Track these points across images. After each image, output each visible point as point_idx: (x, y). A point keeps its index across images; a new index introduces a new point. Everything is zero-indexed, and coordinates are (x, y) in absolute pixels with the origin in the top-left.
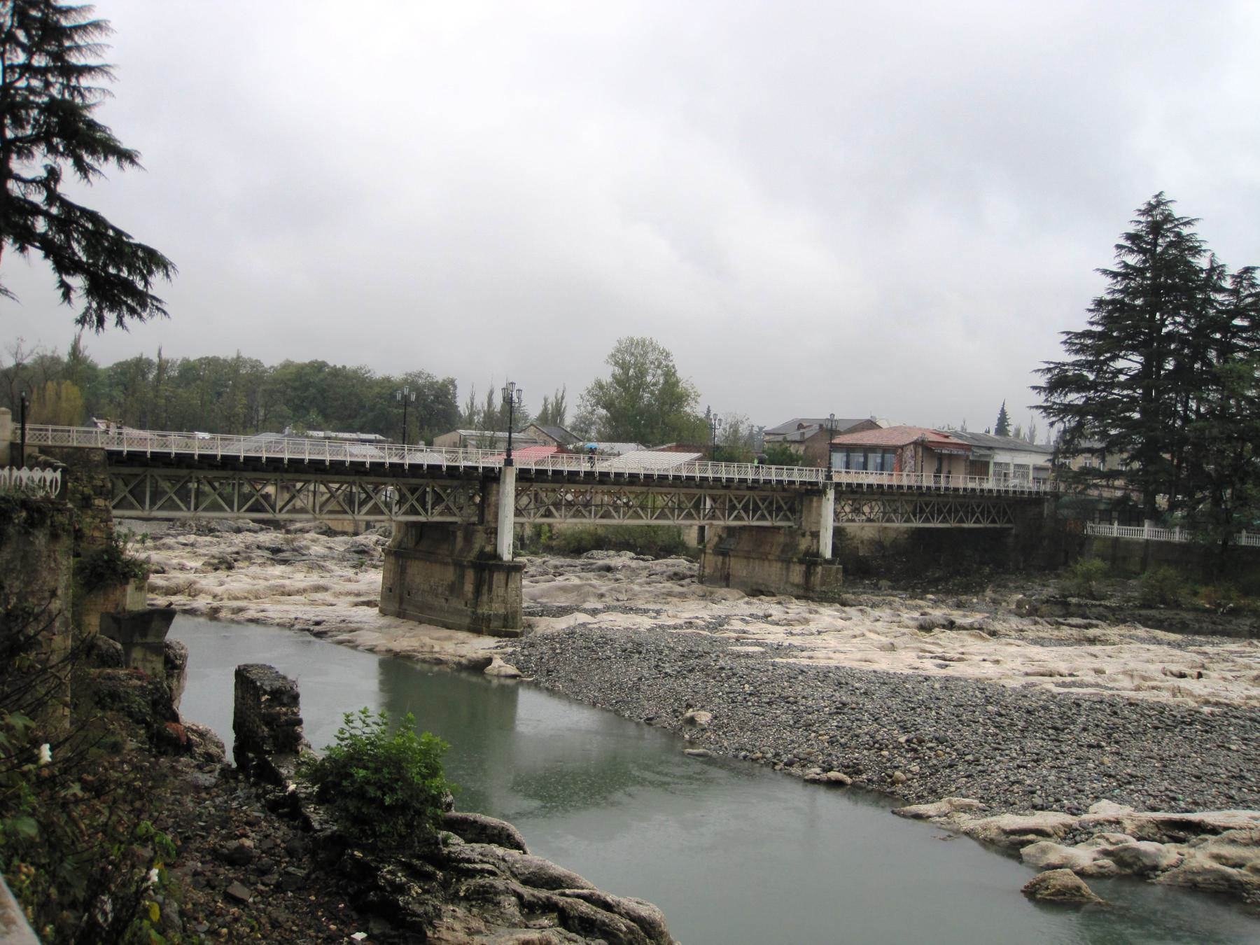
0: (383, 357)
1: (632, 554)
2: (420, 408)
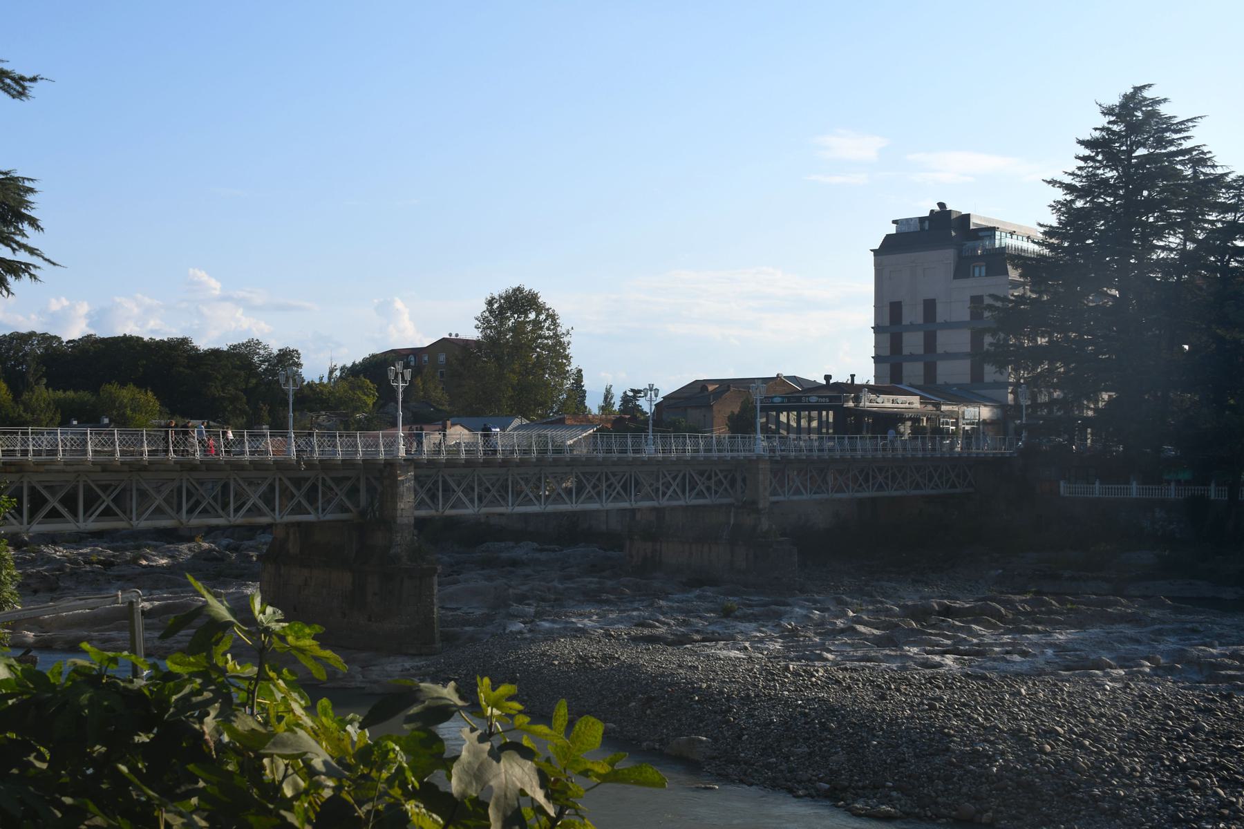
0: (217, 325)
1: (536, 545)
2: (240, 384)
